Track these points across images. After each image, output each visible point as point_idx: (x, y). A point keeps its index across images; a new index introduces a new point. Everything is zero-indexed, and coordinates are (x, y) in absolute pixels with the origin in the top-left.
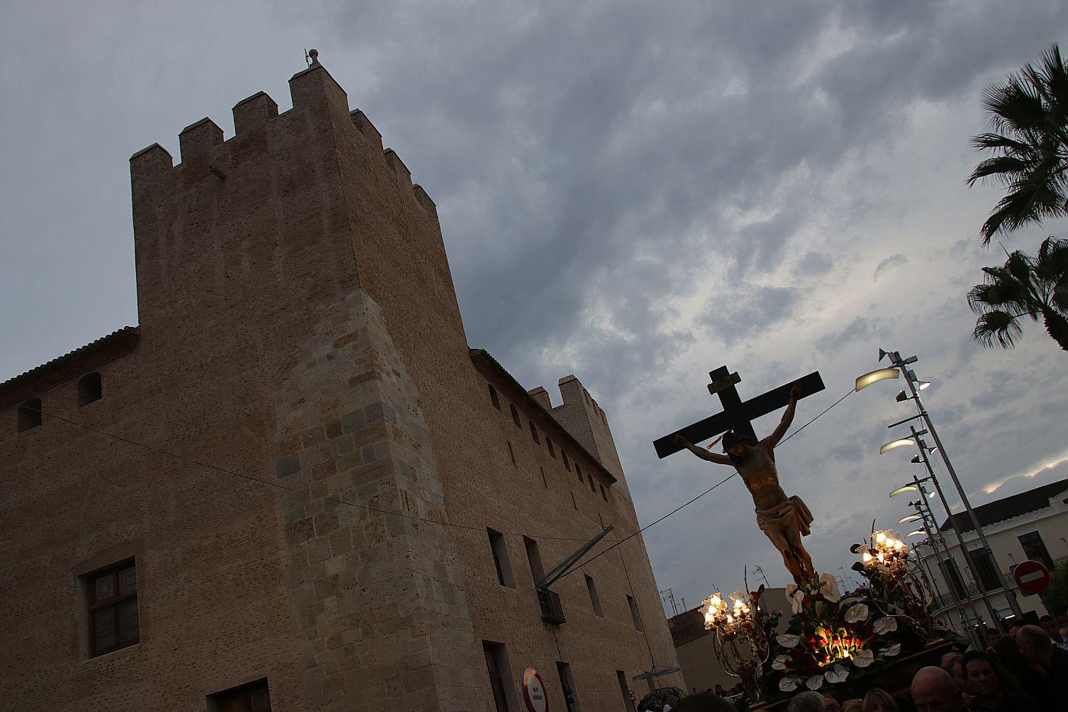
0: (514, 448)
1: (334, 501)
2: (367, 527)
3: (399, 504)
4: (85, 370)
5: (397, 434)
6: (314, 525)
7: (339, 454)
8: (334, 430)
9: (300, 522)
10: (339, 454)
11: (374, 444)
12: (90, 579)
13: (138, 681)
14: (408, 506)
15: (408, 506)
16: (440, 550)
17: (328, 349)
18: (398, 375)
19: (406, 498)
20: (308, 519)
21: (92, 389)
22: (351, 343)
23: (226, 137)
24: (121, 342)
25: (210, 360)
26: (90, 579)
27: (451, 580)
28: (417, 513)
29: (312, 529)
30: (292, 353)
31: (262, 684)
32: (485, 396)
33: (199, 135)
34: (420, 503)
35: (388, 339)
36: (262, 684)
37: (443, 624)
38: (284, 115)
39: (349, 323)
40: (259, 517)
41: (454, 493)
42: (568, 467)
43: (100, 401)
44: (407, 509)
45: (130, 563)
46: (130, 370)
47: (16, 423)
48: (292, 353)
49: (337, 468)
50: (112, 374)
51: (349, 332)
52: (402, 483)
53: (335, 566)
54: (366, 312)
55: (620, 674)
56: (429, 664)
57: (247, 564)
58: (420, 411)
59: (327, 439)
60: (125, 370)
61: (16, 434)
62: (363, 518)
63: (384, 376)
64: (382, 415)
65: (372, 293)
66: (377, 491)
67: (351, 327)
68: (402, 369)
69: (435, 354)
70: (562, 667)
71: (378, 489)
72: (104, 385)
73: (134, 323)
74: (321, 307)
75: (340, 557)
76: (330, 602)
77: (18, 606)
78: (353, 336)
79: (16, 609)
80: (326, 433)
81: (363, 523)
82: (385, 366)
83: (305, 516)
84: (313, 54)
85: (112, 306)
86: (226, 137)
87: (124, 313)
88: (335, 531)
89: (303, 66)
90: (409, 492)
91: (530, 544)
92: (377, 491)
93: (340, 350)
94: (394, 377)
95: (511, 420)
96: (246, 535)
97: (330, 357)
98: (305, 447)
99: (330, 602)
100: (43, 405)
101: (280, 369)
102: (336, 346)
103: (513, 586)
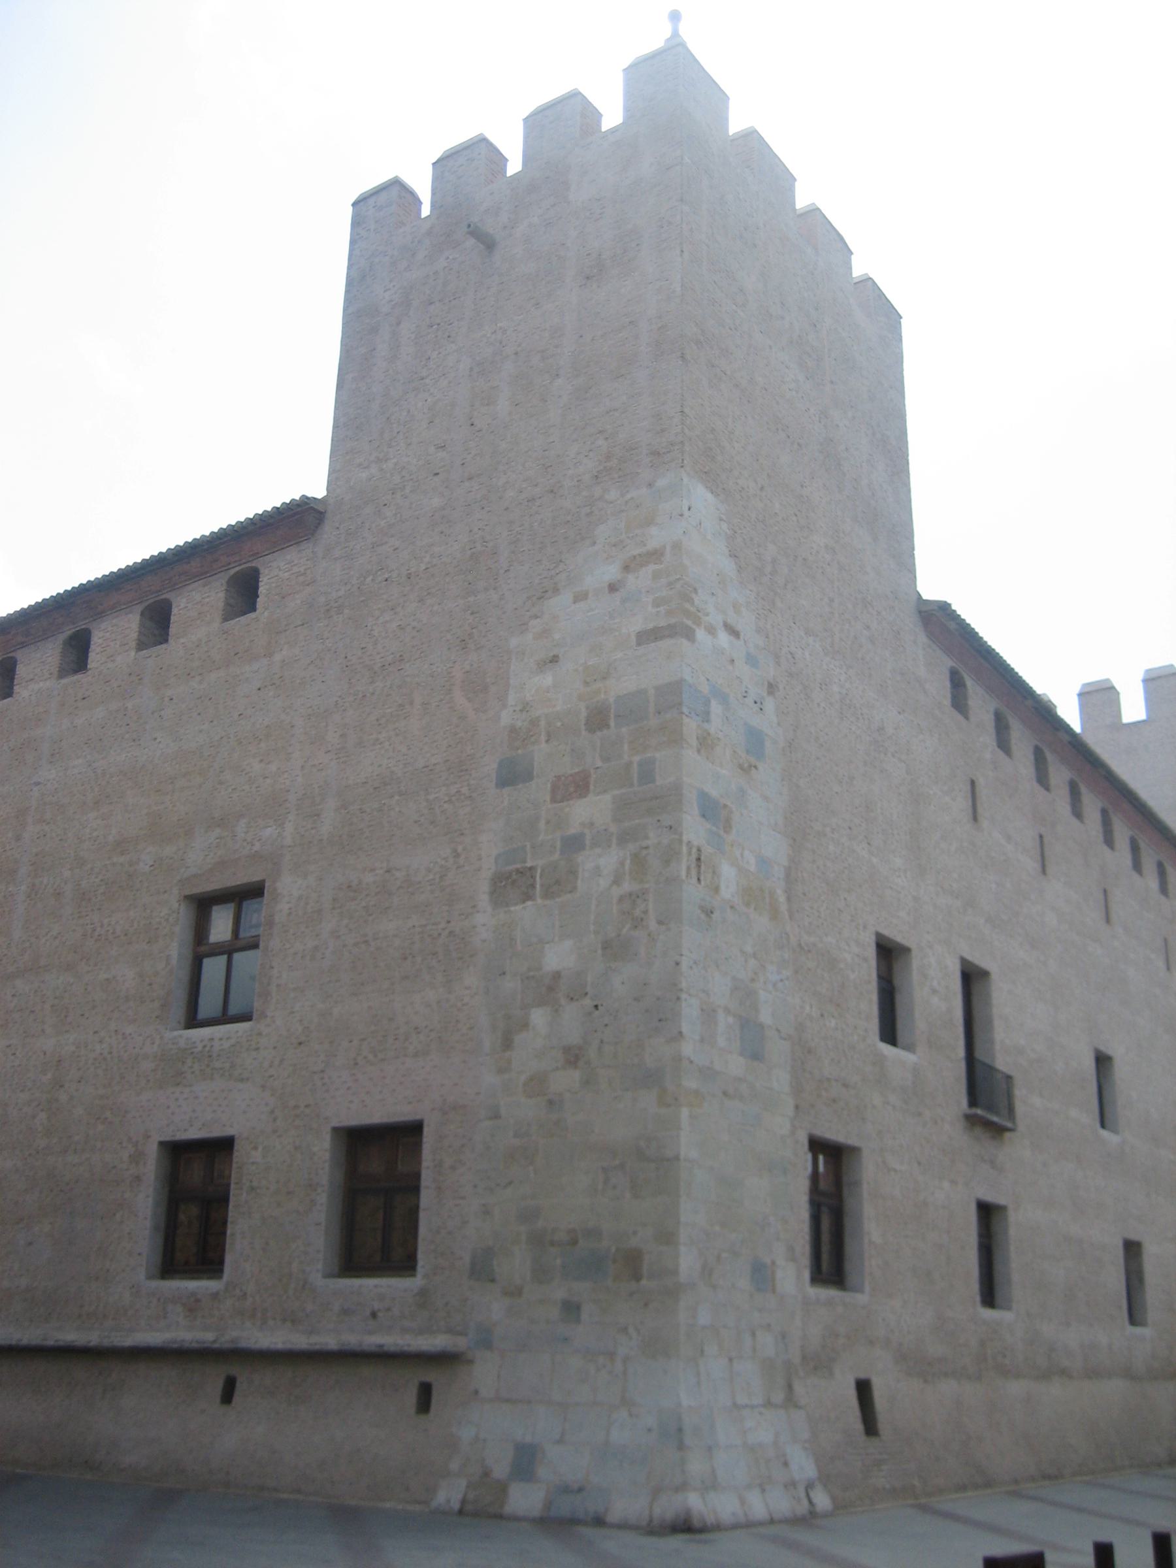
0: (983, 792)
1: (574, 844)
2: (621, 899)
3: (682, 867)
4: (236, 562)
5: (706, 743)
6: (538, 879)
7: (599, 764)
8: (598, 719)
9: (518, 871)
10: (599, 764)
11: (658, 755)
12: (203, 905)
13: (242, 1080)
14: (699, 873)
15: (699, 873)
16: (752, 962)
17: (611, 572)
18: (734, 632)
19: (699, 859)
20: (531, 868)
21: (245, 593)
22: (652, 567)
23: (607, 124)
24: (293, 523)
25: (423, 567)
26: (203, 905)
27: (765, 1017)
28: (717, 890)
29: (533, 886)
30: (553, 572)
31: (415, 1129)
32: (940, 688)
33: (468, 163)
34: (727, 872)
35: (728, 566)
36: (415, 1129)
37: (725, 1094)
38: (613, 131)
39: (654, 530)
40: (455, 851)
41: (814, 861)
42: (1109, 841)
43: (252, 615)
44: (694, 880)
45: (255, 891)
46: (302, 569)
47: (134, 635)
48: (553, 572)
49: (592, 787)
50: (278, 572)
51: (652, 544)
52: (694, 830)
53: (559, 957)
54: (686, 513)
55: (1132, 1249)
56: (677, 1158)
57: (425, 926)
58: (770, 704)
59: (584, 733)
60: (295, 569)
61: (133, 653)
62: (617, 881)
63: (700, 634)
64: (680, 704)
65: (711, 479)
66: (647, 838)
67: (656, 537)
68: (746, 622)
69: (831, 600)
70: (987, 1213)
71: (651, 835)
72: (262, 590)
73: (318, 491)
74: (613, 494)
75: (568, 944)
76: (539, 1017)
77: (102, 926)
78: (656, 555)
79: (98, 929)
80: (583, 722)
81: (616, 892)
82: (707, 615)
83: (525, 862)
84: (675, 17)
85: (282, 455)
86: (607, 124)
87: (300, 469)
88: (569, 896)
89: (654, 40)
90: (708, 850)
91: (972, 979)
92: (647, 838)
93: (631, 578)
94: (723, 638)
95: (988, 739)
96: (431, 877)
97: (613, 588)
98: (547, 741)
99: (539, 1017)
100: (175, 611)
101: (528, 598)
102: (626, 568)
103: (910, 1048)
